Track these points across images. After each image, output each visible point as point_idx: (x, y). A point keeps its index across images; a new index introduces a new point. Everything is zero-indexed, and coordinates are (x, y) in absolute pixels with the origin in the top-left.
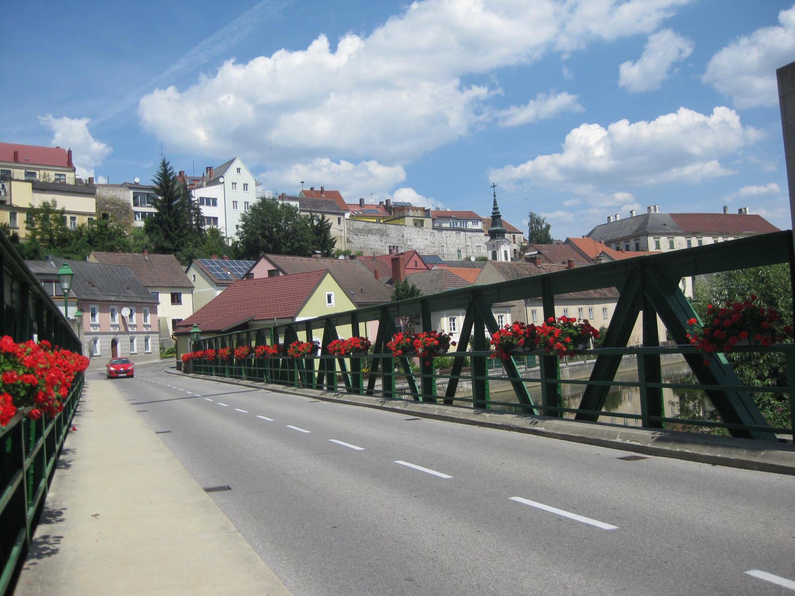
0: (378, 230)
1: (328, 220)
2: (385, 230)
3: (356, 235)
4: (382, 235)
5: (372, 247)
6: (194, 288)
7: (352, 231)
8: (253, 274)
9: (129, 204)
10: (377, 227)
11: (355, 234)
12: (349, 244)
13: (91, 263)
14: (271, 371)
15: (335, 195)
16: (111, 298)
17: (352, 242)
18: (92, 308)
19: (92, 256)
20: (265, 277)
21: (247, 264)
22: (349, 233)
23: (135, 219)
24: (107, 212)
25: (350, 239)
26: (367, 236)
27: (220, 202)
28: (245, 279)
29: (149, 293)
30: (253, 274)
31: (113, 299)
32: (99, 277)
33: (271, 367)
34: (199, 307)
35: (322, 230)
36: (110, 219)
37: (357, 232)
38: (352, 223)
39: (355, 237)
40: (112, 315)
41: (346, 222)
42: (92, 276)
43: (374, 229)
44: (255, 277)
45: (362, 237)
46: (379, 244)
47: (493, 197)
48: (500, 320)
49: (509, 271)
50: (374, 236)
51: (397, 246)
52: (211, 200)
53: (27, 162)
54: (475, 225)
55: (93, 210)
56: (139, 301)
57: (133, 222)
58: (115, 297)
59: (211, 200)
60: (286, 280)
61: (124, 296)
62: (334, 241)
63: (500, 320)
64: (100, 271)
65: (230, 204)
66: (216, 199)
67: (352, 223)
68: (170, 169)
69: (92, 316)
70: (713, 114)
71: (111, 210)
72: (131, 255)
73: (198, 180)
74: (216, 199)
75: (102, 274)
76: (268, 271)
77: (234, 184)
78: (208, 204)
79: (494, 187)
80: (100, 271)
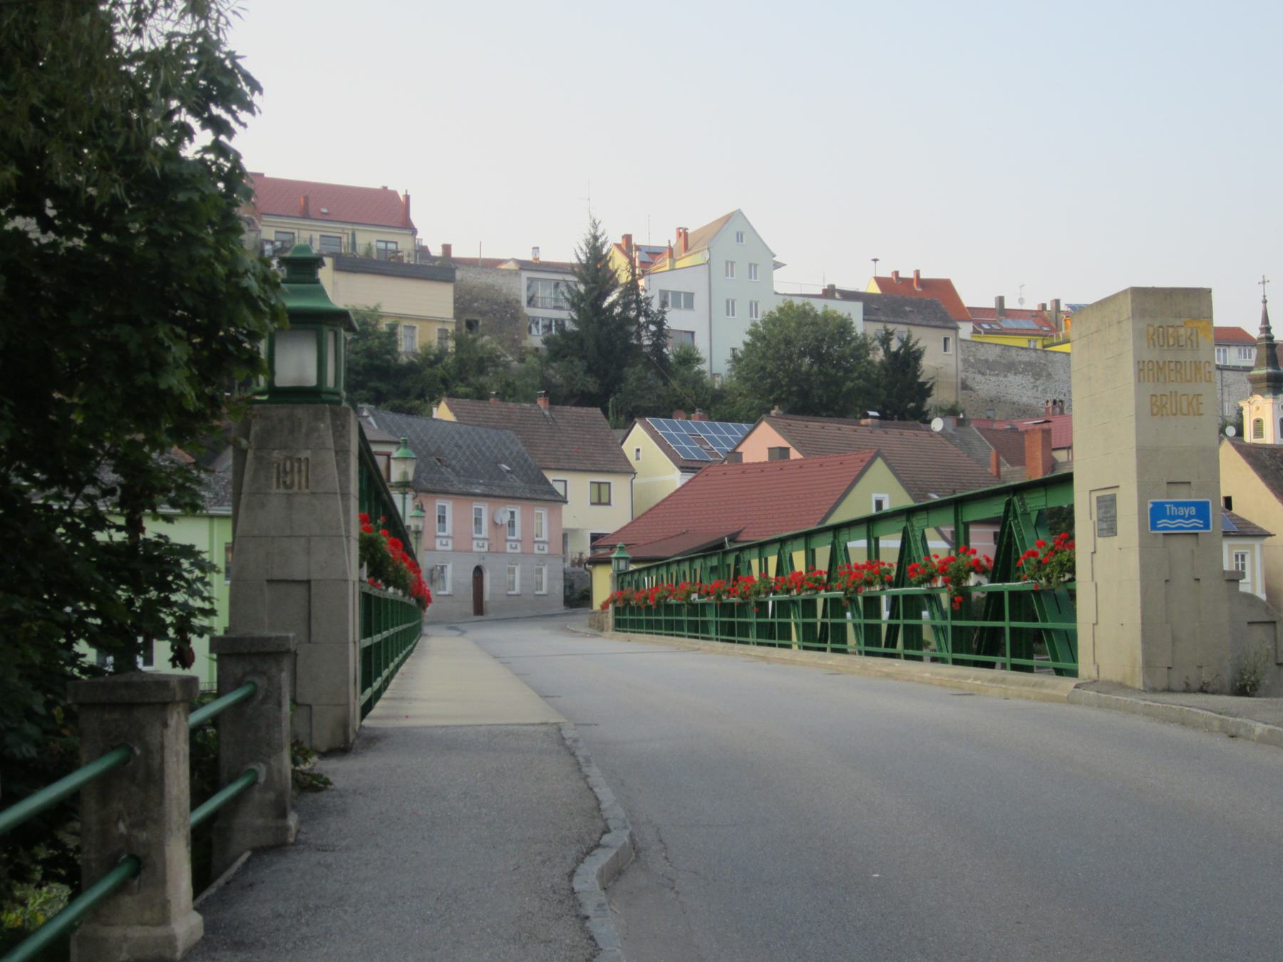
0: (1029, 364)
1: (917, 342)
2: (1045, 365)
3: (983, 374)
4: (1037, 376)
5: (1015, 399)
6: (635, 474)
7: (972, 366)
8: (741, 453)
9: (518, 302)
10: (1027, 359)
11: (980, 372)
12: (965, 392)
13: (441, 421)
14: (717, 622)
15: (943, 288)
16: (477, 488)
17: (971, 389)
18: (439, 506)
19: (443, 405)
20: (763, 460)
21: (741, 429)
22: (966, 370)
23: (530, 332)
24: (476, 318)
25: (969, 382)
26: (1006, 376)
27: (700, 301)
28: (726, 463)
29: (547, 482)
30: (741, 453)
31: (478, 491)
32: (456, 449)
33: (716, 616)
34: (638, 513)
35: (907, 360)
36: (480, 330)
37: (987, 367)
38: (974, 349)
39: (979, 377)
40: (571, 587)
41: (961, 346)
42: (443, 446)
43: (1020, 362)
44: (745, 460)
45: (993, 379)
46: (1030, 393)
47: (1262, 305)
48: (1240, 562)
49: (1268, 463)
50: (1021, 376)
51: (1061, 401)
52: (682, 296)
53: (327, 218)
54: (1245, 357)
55: (447, 311)
56: (529, 496)
57: (526, 338)
58: (482, 487)
59: (682, 296)
60: (762, 471)
61: (499, 486)
62: (928, 386)
63: (1240, 562)
64: (457, 437)
65: (719, 307)
66: (692, 294)
67: (974, 349)
68: (603, 234)
69: (439, 521)
70: (192, 547)
71: (483, 314)
72: (518, 407)
73: (129, 761)
74: (692, 294)
75: (460, 442)
76: (769, 449)
77: (730, 265)
78: (677, 305)
79: (1264, 282)
80: (457, 437)
